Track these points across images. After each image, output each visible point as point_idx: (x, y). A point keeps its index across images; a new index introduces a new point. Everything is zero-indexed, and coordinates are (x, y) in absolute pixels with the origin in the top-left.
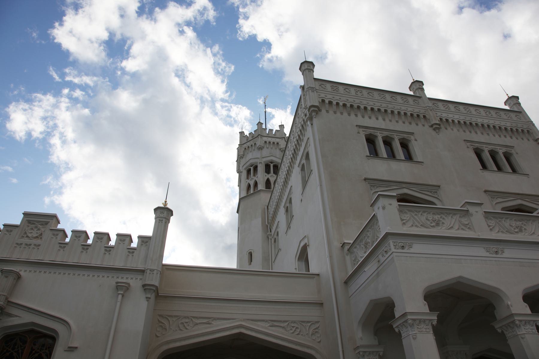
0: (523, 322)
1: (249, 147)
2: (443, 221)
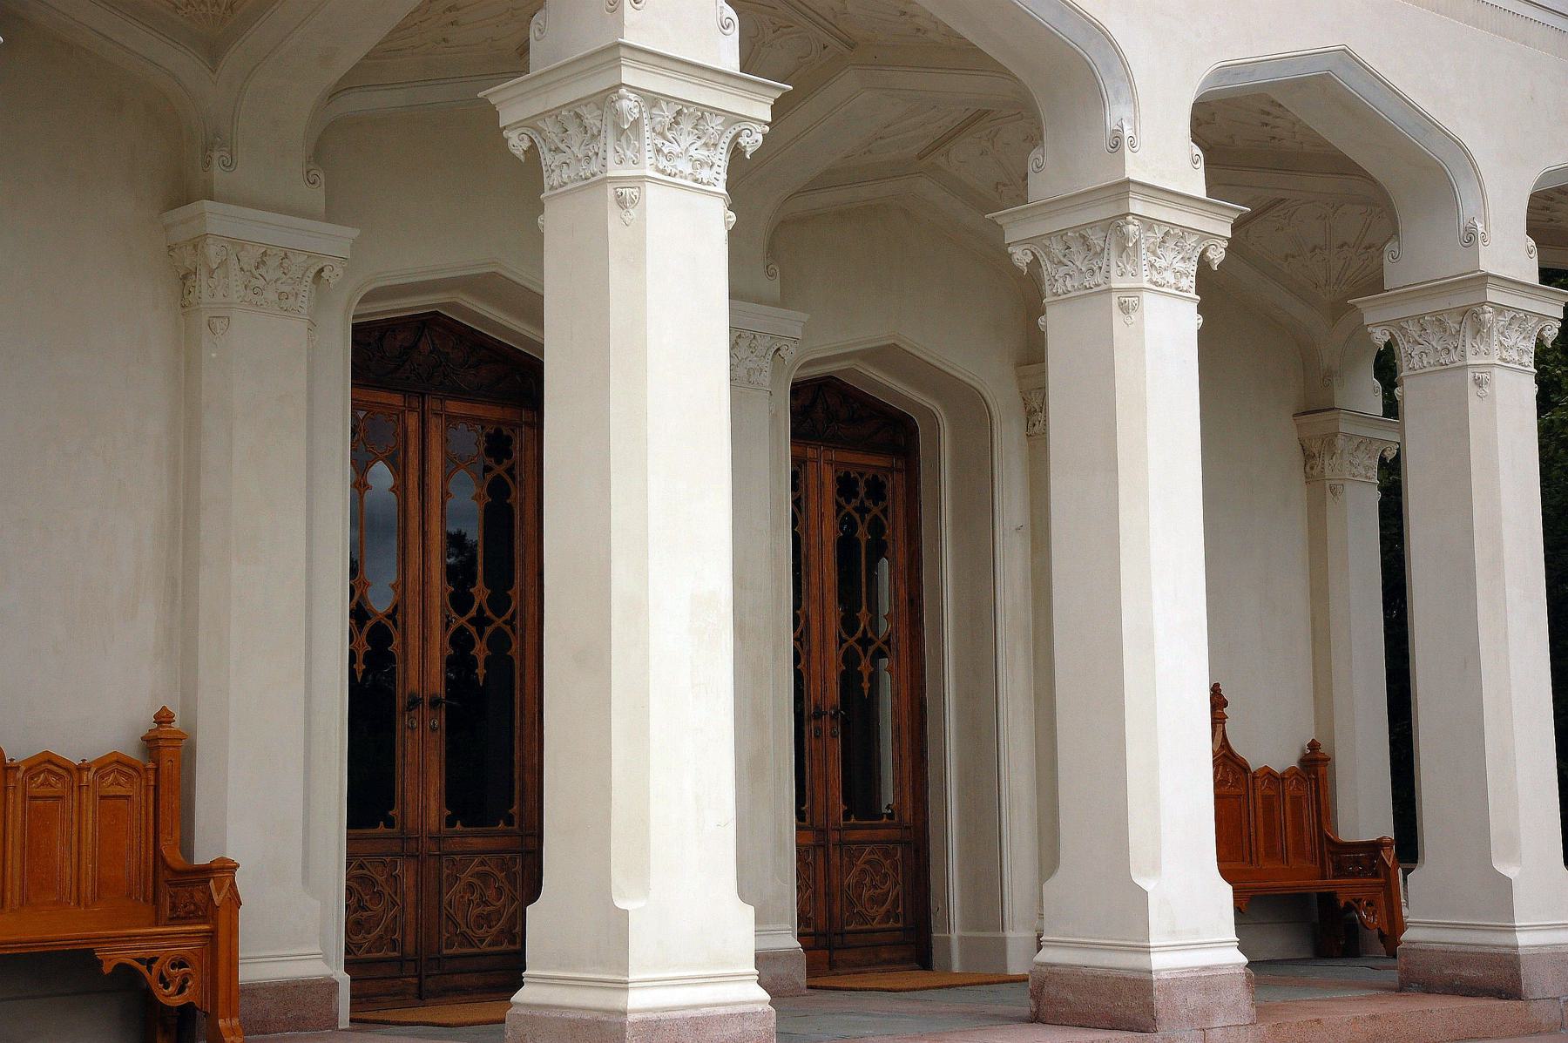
0: (668, 114)
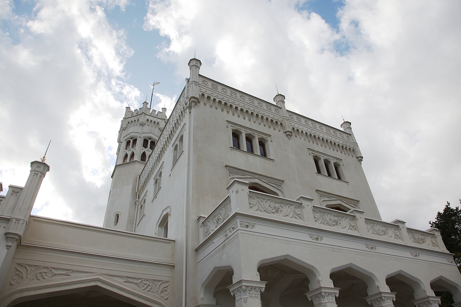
0: (327, 294)
1: (132, 121)
2: (282, 209)
